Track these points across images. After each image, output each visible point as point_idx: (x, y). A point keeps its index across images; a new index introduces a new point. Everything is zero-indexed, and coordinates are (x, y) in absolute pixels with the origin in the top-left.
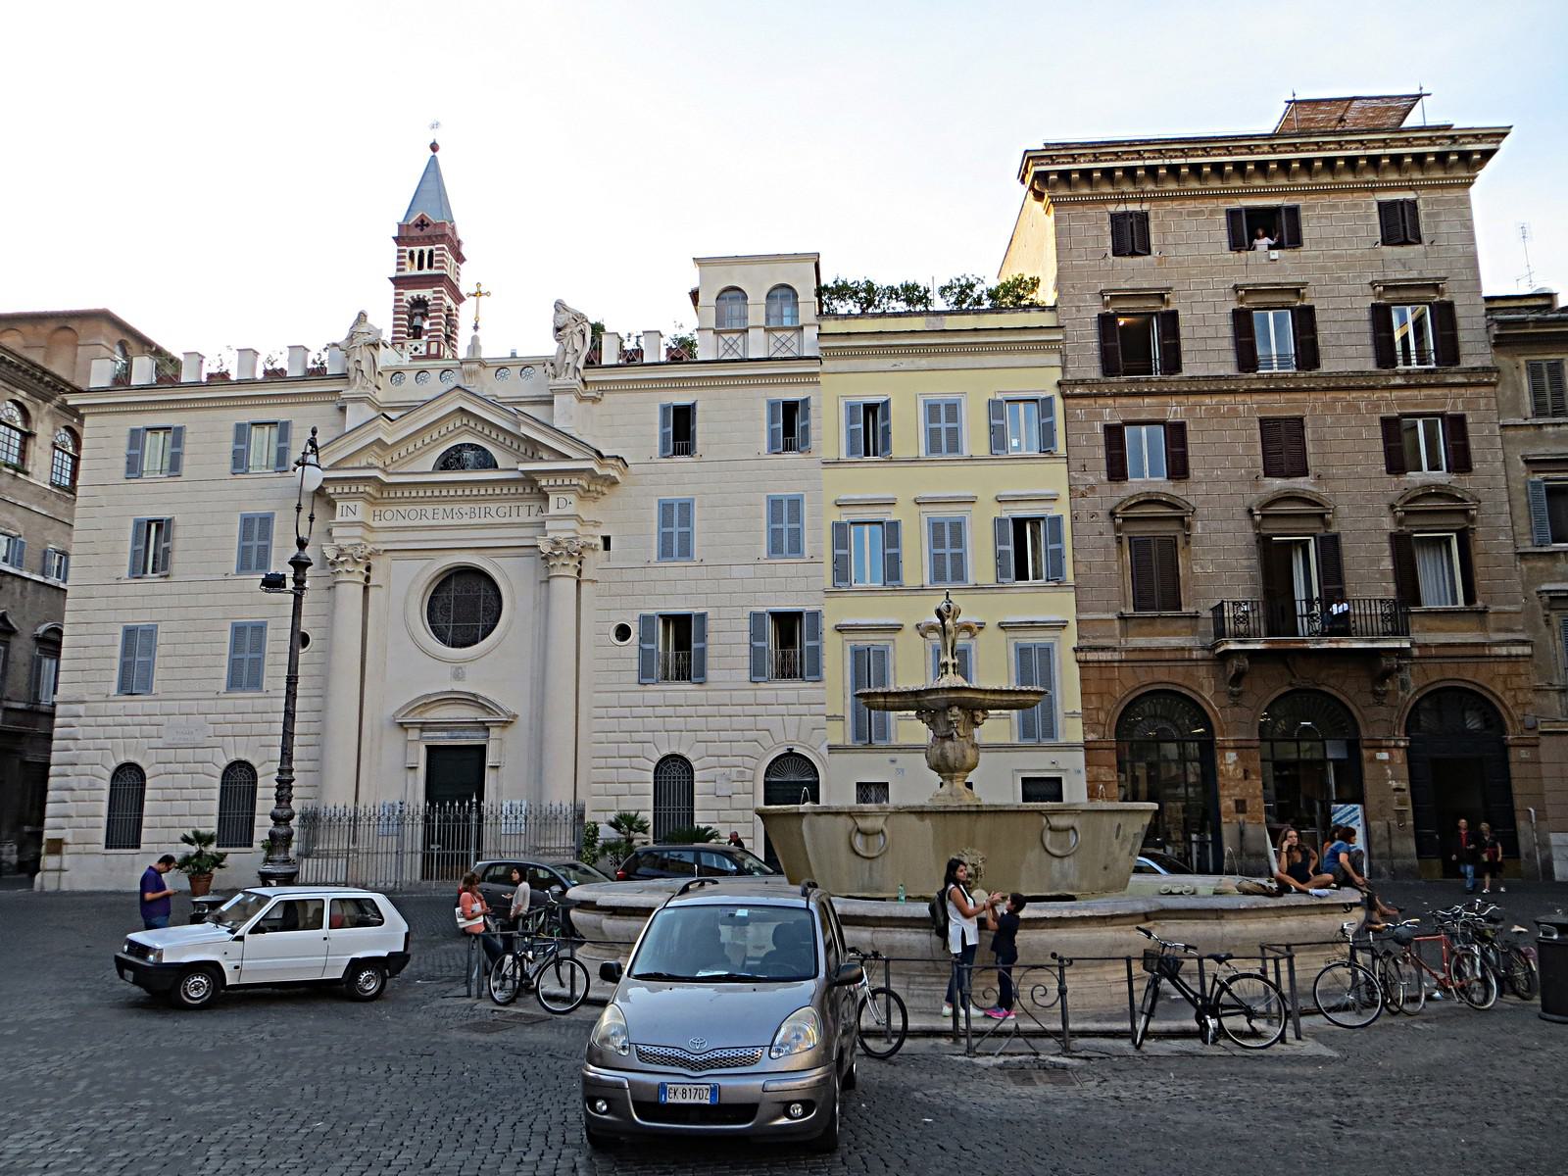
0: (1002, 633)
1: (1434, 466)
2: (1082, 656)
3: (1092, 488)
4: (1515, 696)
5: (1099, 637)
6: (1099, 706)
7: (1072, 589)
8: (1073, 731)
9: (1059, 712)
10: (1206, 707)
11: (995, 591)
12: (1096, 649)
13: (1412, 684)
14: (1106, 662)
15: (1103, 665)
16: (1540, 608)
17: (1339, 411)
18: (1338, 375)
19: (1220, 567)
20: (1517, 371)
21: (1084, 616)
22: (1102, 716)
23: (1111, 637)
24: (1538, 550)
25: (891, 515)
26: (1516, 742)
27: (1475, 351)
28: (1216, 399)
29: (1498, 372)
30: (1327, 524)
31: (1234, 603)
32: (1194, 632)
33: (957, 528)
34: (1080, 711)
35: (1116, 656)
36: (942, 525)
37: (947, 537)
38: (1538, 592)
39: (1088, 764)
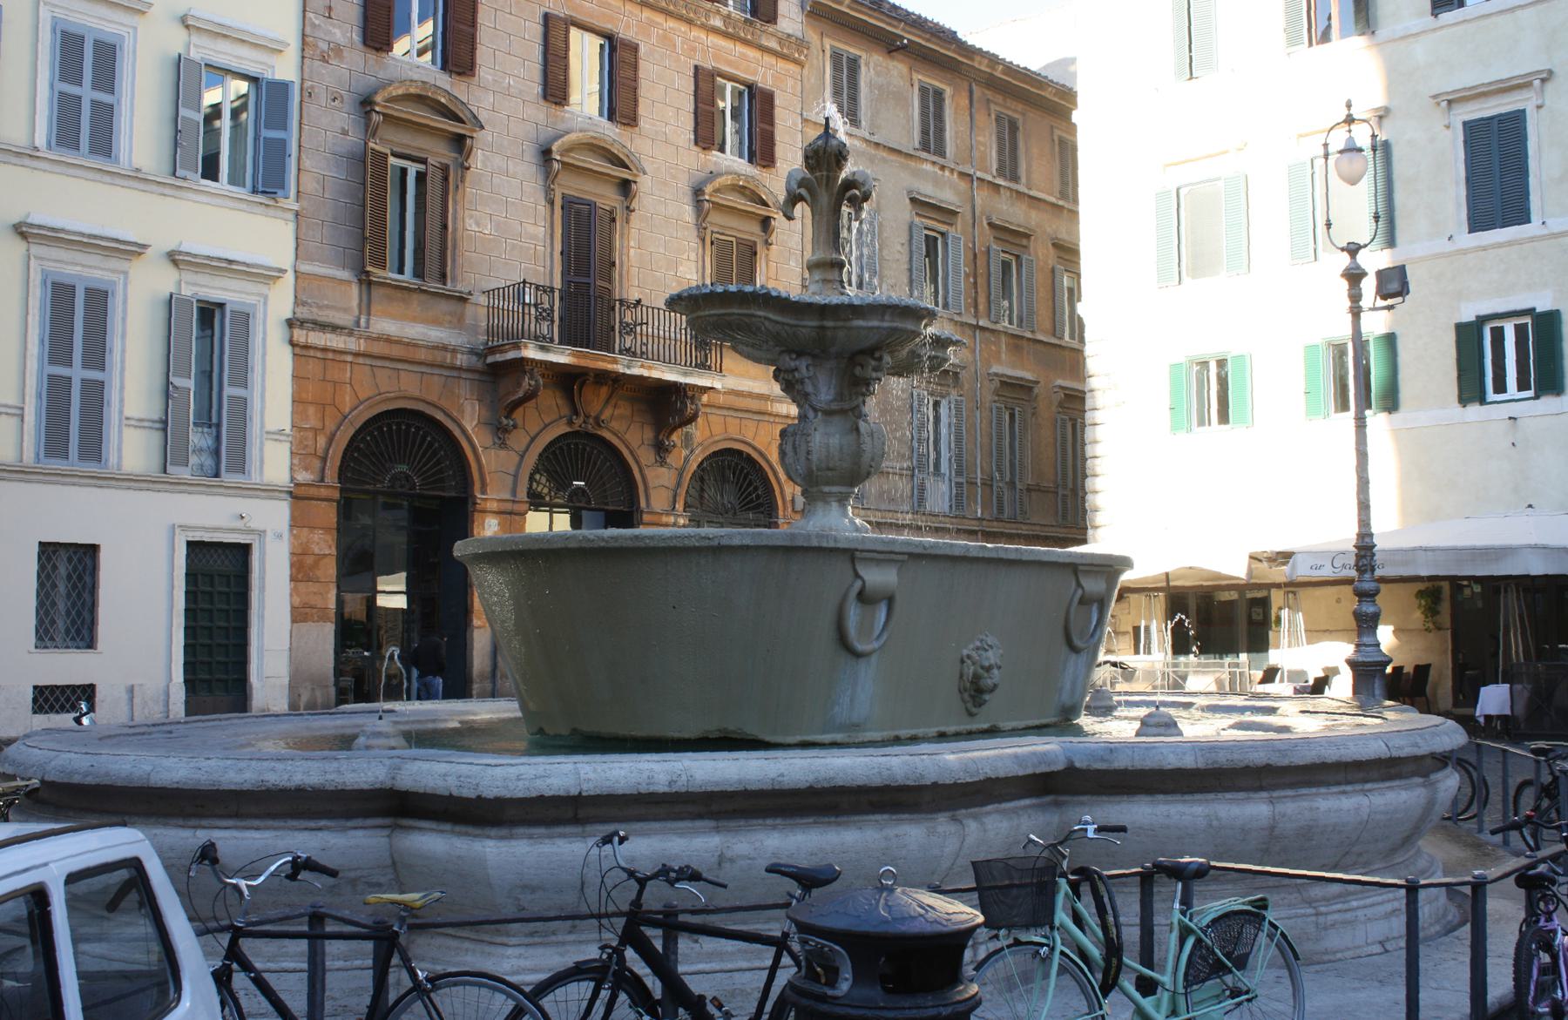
2: (300, 335)
3: (338, 50)
5: (327, 307)
6: (319, 425)
7: (291, 216)
8: (274, 461)
9: (254, 430)
10: (464, 444)
11: (167, 191)
14: (334, 351)
15: (330, 356)
17: (654, 40)
19: (506, 232)
21: (305, 268)
23: (346, 310)
31: (537, 287)
32: (459, 322)
34: (288, 431)
35: (352, 344)
39: (295, 523)
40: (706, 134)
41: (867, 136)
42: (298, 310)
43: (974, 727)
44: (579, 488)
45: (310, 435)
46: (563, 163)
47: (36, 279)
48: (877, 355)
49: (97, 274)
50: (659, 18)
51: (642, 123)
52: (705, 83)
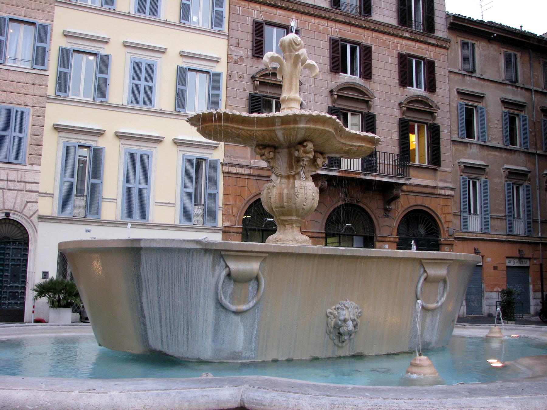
0: (175, 148)
1: (352, 73)
4: (445, 217)
5: (238, 157)
9: (217, 207)
12: (236, 165)
13: (403, 205)
16: (459, 172)
17: (378, 44)
18: (381, 24)
20: (456, 41)
22: (235, 210)
23: (245, 158)
24: (460, 140)
25: (104, 50)
26: (445, 242)
27: (441, 29)
28: (317, 21)
29: (450, 42)
30: (369, 107)
33: (150, 68)
35: (247, 171)
36: (140, 64)
37: (143, 73)
38: (459, 163)
40: (405, 80)
41: (479, 76)
42: (225, 159)
43: (341, 353)
44: (349, 227)
45: (230, 207)
46: (338, 96)
47: (123, 152)
48: (305, 144)
49: (145, 149)
50: (381, 35)
51: (374, 77)
52: (404, 61)
